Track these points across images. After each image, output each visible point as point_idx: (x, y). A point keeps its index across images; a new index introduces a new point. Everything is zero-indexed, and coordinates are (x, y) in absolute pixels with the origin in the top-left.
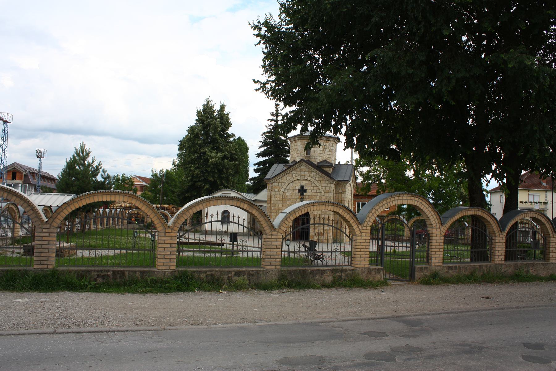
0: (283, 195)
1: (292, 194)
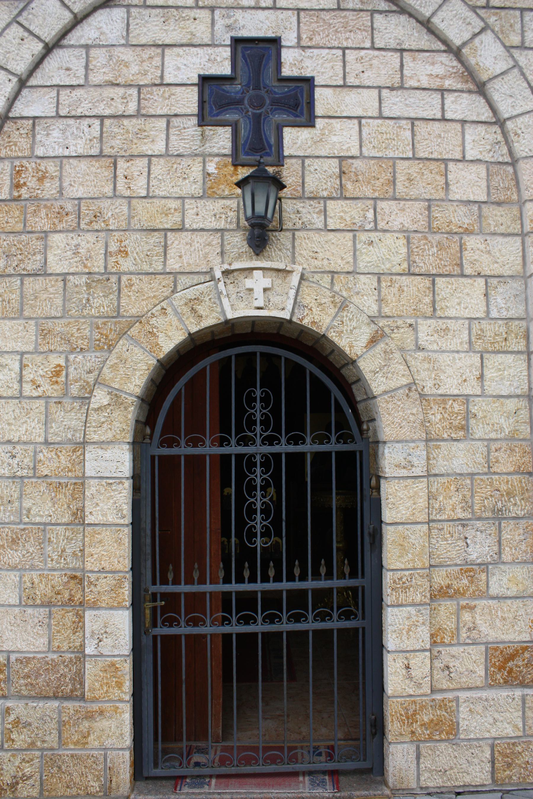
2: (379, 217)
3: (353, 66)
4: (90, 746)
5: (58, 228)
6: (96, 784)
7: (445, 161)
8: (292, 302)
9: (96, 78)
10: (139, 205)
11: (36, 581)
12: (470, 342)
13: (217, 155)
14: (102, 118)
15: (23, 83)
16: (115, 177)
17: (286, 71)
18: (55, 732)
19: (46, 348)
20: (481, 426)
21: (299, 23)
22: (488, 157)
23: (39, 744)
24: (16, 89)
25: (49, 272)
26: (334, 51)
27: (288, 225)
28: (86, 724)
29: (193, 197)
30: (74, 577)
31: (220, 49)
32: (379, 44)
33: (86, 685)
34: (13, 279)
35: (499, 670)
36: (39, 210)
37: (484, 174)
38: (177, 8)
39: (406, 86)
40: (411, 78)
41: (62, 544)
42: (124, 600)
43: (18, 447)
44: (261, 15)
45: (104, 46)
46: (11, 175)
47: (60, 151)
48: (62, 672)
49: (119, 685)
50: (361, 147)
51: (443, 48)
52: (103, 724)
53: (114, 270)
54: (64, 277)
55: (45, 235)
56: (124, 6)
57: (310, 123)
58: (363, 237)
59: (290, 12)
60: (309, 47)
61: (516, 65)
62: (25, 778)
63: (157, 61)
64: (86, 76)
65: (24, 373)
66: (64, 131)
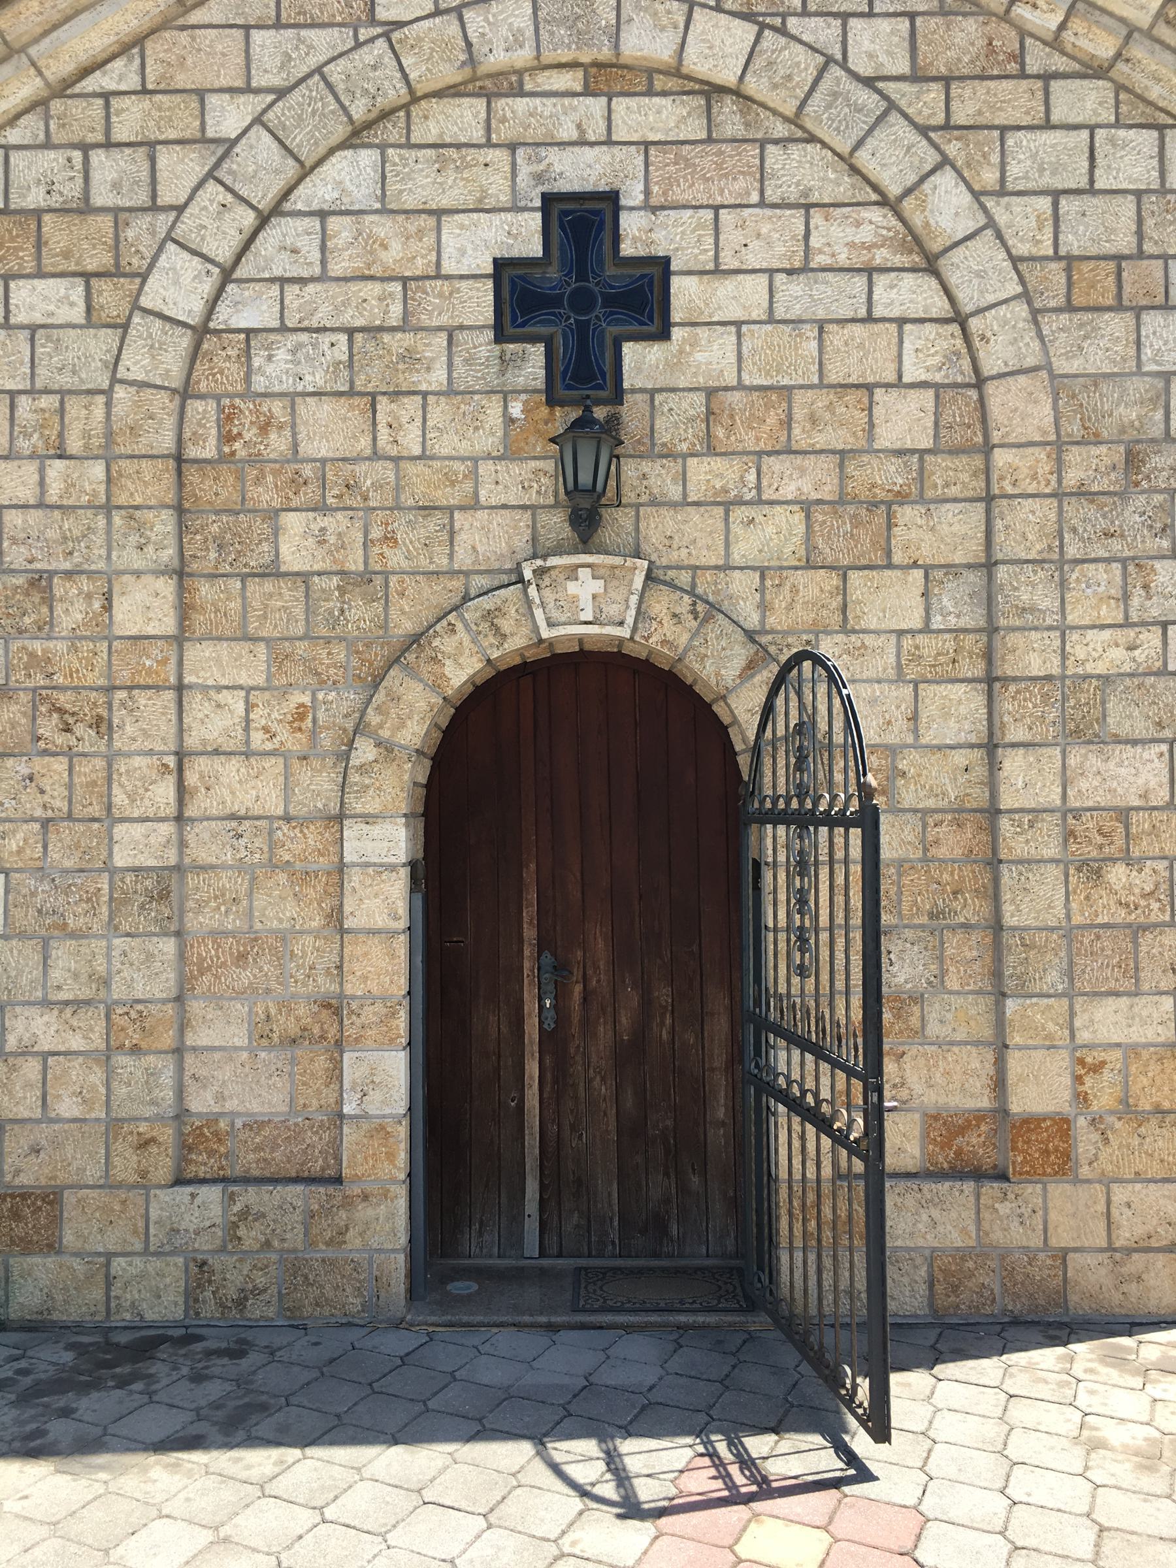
0: (185, 393)
1: (370, 378)
2: (765, 483)
3: (731, 236)
4: (350, 1247)
5: (293, 505)
6: (358, 1301)
7: (869, 388)
8: (633, 612)
9: (337, 268)
10: (411, 468)
11: (273, 1012)
12: (899, 666)
13: (525, 391)
14: (351, 332)
15: (227, 275)
16: (374, 424)
17: (627, 249)
18: (300, 1229)
19: (284, 681)
20: (912, 787)
21: (647, 164)
22: (938, 378)
23: (276, 1243)
24: (217, 285)
25: (283, 569)
26: (702, 212)
27: (629, 496)
28: (343, 1214)
29: (489, 457)
30: (328, 1006)
31: (526, 215)
32: (772, 195)
33: (345, 1158)
34: (231, 581)
35: (942, 1148)
36: (264, 477)
37: (930, 405)
38: (458, 146)
39: (812, 265)
40: (820, 252)
41: (310, 959)
42: (399, 1036)
43: (247, 823)
44: (589, 153)
45: (348, 213)
46: (218, 420)
47: (288, 385)
48: (308, 1141)
49: (391, 1156)
50: (739, 371)
51: (874, 197)
52: (364, 1212)
53: (378, 568)
54: (304, 577)
55: (273, 515)
56: (377, 146)
57: (664, 334)
58: (739, 513)
59: (633, 148)
60: (663, 208)
61: (991, 223)
62: (258, 1292)
63: (429, 240)
64: (324, 262)
65: (252, 716)
66: (293, 352)
